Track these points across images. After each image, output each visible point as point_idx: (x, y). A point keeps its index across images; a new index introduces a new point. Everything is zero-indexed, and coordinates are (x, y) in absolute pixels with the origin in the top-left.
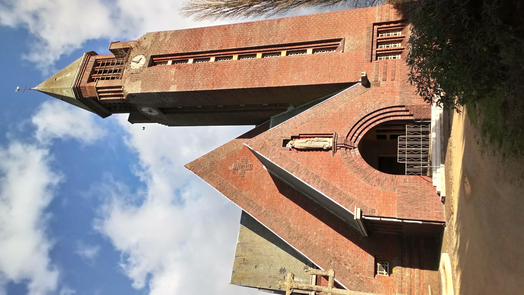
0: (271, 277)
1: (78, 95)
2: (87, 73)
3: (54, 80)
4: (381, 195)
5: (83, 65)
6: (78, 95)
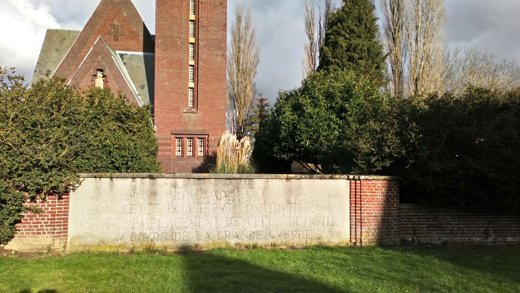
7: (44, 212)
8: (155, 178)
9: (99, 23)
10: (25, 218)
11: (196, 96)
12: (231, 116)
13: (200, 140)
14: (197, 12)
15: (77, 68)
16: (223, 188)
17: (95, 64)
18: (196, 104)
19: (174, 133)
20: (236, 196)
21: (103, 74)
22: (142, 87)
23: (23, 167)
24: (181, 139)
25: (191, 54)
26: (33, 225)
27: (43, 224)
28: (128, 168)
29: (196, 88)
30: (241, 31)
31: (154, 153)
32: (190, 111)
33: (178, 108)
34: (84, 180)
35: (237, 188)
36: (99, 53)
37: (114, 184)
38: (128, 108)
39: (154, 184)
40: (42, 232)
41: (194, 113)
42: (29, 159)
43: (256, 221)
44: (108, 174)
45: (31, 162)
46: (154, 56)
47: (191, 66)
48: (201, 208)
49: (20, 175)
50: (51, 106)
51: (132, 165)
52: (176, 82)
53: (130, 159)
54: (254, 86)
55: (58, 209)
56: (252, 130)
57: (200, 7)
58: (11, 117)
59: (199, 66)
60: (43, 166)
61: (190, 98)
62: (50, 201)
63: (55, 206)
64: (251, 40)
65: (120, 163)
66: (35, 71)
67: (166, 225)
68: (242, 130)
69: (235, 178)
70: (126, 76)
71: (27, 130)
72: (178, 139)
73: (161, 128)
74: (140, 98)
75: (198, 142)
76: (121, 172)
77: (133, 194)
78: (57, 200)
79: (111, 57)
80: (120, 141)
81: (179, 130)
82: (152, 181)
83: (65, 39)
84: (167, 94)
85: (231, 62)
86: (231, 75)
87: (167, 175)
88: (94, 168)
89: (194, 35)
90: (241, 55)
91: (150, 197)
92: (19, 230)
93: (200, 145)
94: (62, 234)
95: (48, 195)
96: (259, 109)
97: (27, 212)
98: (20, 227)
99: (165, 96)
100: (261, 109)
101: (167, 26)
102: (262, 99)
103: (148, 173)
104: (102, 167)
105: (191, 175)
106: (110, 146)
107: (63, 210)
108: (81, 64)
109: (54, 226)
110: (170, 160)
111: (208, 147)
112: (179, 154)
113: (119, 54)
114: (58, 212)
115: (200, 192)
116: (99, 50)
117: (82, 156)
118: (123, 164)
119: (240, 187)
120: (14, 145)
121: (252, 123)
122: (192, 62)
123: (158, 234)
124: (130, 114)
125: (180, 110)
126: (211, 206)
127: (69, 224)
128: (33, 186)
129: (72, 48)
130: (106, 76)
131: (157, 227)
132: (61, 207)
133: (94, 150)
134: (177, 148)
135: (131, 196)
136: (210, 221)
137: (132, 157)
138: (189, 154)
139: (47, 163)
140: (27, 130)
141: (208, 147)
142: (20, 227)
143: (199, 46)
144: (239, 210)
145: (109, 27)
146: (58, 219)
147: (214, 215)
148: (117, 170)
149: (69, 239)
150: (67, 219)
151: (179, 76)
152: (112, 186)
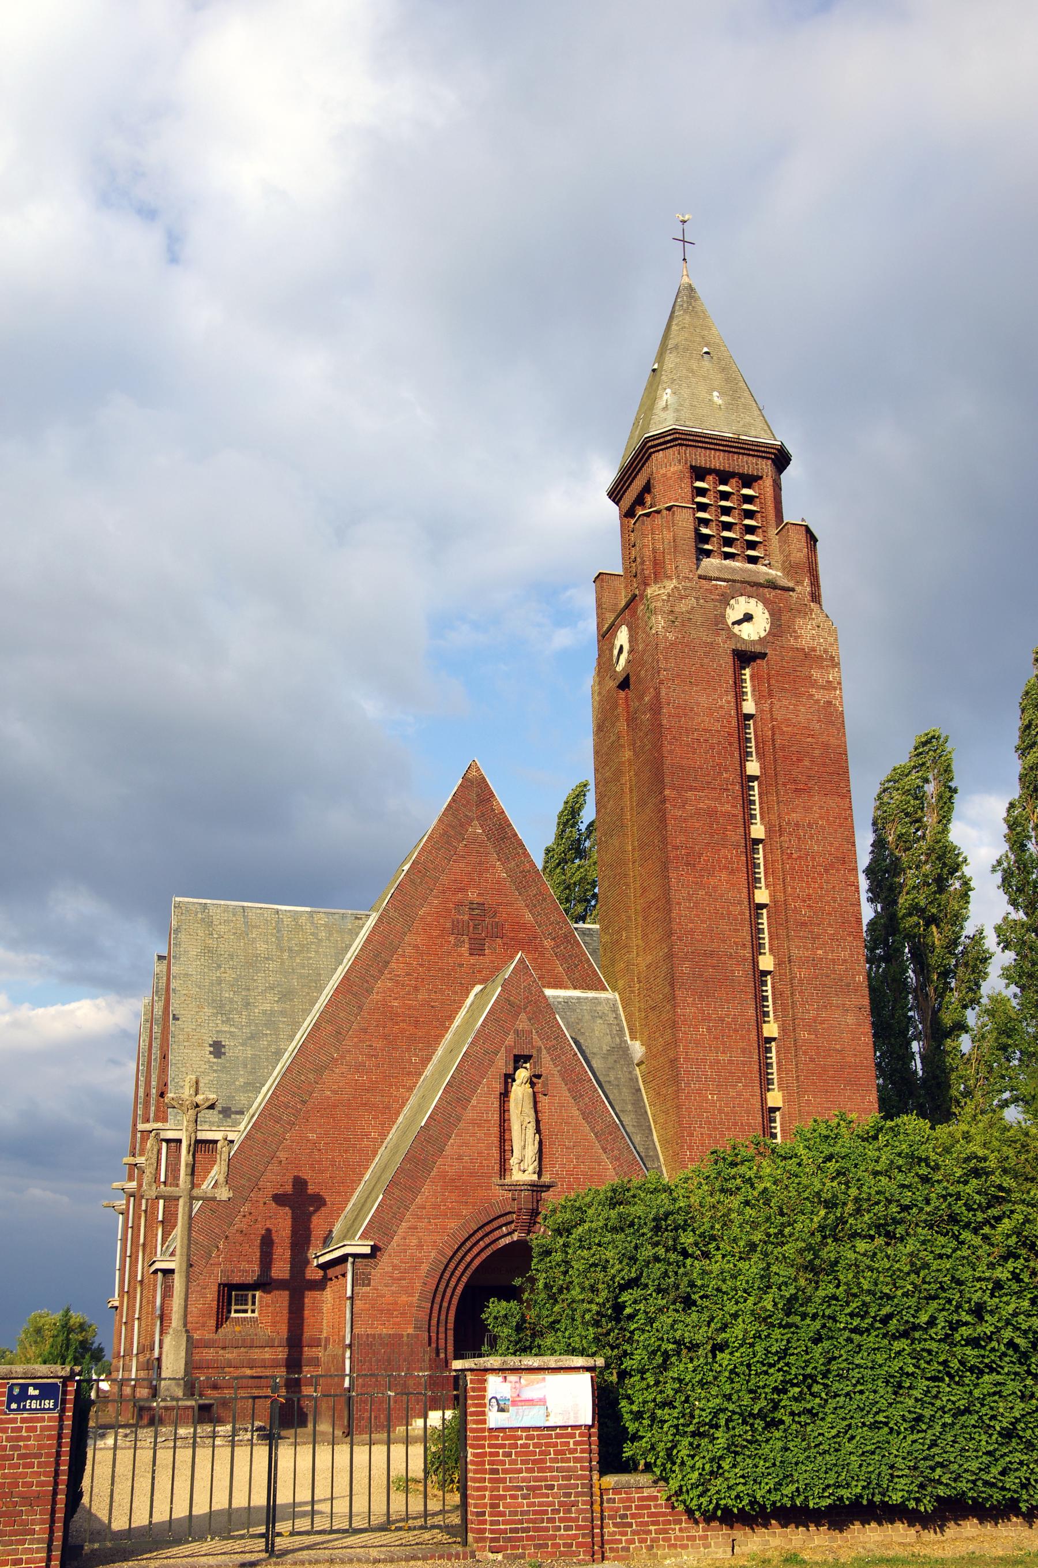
2: (717, 460)
3: (705, 349)
4: (404, 1298)
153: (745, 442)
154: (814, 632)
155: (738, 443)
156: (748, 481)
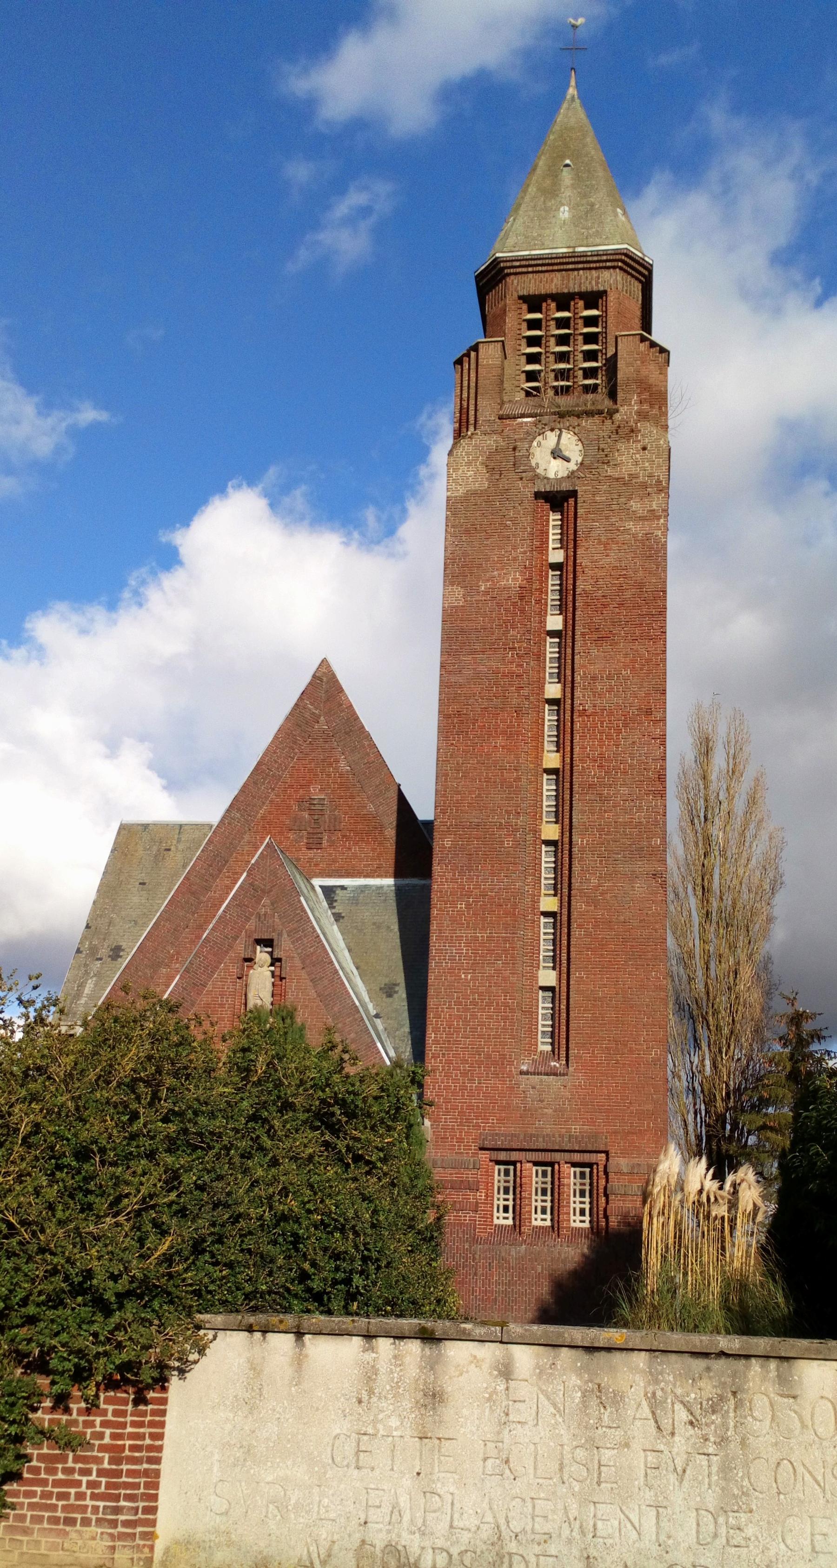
0: (109, 926)
1: (484, 281)
2: (555, 283)
5: (580, 256)
6: (484, 281)
7: (89, 1446)
8: (440, 1340)
9: (266, 798)
10: (34, 1463)
11: (564, 1015)
12: (684, 1077)
13: (578, 1170)
14: (568, 743)
15: (200, 938)
16: (679, 1391)
17: (251, 924)
18: (564, 1042)
19: (487, 1144)
20: (732, 1424)
21: (271, 954)
22: (389, 991)
23: (40, 1293)
24: (511, 1168)
25: (547, 876)
26: (56, 1490)
27: (84, 1488)
28: (352, 1297)
29: (564, 989)
30: (713, 786)
31: (432, 1238)
32: (542, 1069)
33: (503, 1057)
34: (215, 1338)
35: (734, 1393)
36: (263, 891)
37: (306, 1356)
38: (353, 1085)
39: (437, 1362)
40: (79, 1516)
41: (555, 1074)
42: (62, 1266)
43: (812, 1535)
44: (290, 1320)
45: (67, 1278)
46: (427, 889)
47: (546, 914)
48: (600, 1465)
49: (31, 1320)
50: (133, 1092)
51: (364, 1287)
52: (498, 971)
53: (358, 1265)
54: (766, 968)
55: (132, 1436)
56: (764, 1127)
57: (577, 726)
58: (24, 1129)
59: (574, 915)
60: (102, 1294)
61: (543, 1024)
62: (111, 1408)
63: (123, 1425)
64: (748, 813)
65: (325, 1279)
66: (79, 951)
67: (477, 1522)
68: (728, 1127)
69: (722, 1354)
70: (340, 956)
71: (62, 1171)
72: (502, 1167)
73: (445, 1129)
74: (380, 1027)
75: (571, 1177)
76: (329, 1312)
77: (365, 1397)
78: (130, 1407)
79: (300, 901)
80: (327, 1201)
81: (505, 1135)
82: (427, 1351)
83: (169, 850)
84: (466, 1010)
85: (681, 890)
86: (681, 935)
87: (480, 1331)
88: (248, 1297)
89: (557, 816)
90: (715, 860)
91: (423, 1411)
92: (13, 1507)
93: (578, 1188)
94: (139, 1529)
95: (106, 1390)
96: (787, 1050)
97: (39, 1445)
98: (16, 1494)
99: (460, 1017)
100: (794, 1049)
101: (470, 793)
102: (797, 1012)
103: (415, 1321)
104: (270, 1292)
105: (560, 1335)
106: (297, 1220)
107: (148, 1441)
108: (211, 926)
109: (117, 1498)
110: (475, 1240)
111: (606, 1195)
112: (503, 1220)
113: (321, 887)
114: (133, 1448)
115: (594, 1402)
116: (263, 879)
117: (213, 1255)
118: (335, 1282)
119: (743, 1391)
120: (23, 1223)
121: (764, 1102)
122: (549, 903)
123: (450, 1556)
124: (360, 1103)
125: (511, 1063)
126: (638, 1460)
127: (162, 1493)
128: (65, 1359)
129: (187, 878)
130: (279, 960)
131: (443, 1526)
132: (142, 1430)
133: (250, 1233)
134: (499, 1200)
135: (360, 1402)
136: (635, 1520)
137: (365, 1259)
138: (540, 1220)
139: (111, 1284)
140: (62, 1171)
141: (606, 1195)
142: (16, 1494)
143: (575, 850)
144: (746, 1483)
145: (295, 808)
146: (130, 1473)
147: (649, 1495)
148: (315, 1301)
149: (160, 1546)
150: (157, 1473)
151: (505, 951)
152: (299, 1362)
153: (584, 255)
154: (638, 456)
155: (574, 257)
156: (593, 299)
